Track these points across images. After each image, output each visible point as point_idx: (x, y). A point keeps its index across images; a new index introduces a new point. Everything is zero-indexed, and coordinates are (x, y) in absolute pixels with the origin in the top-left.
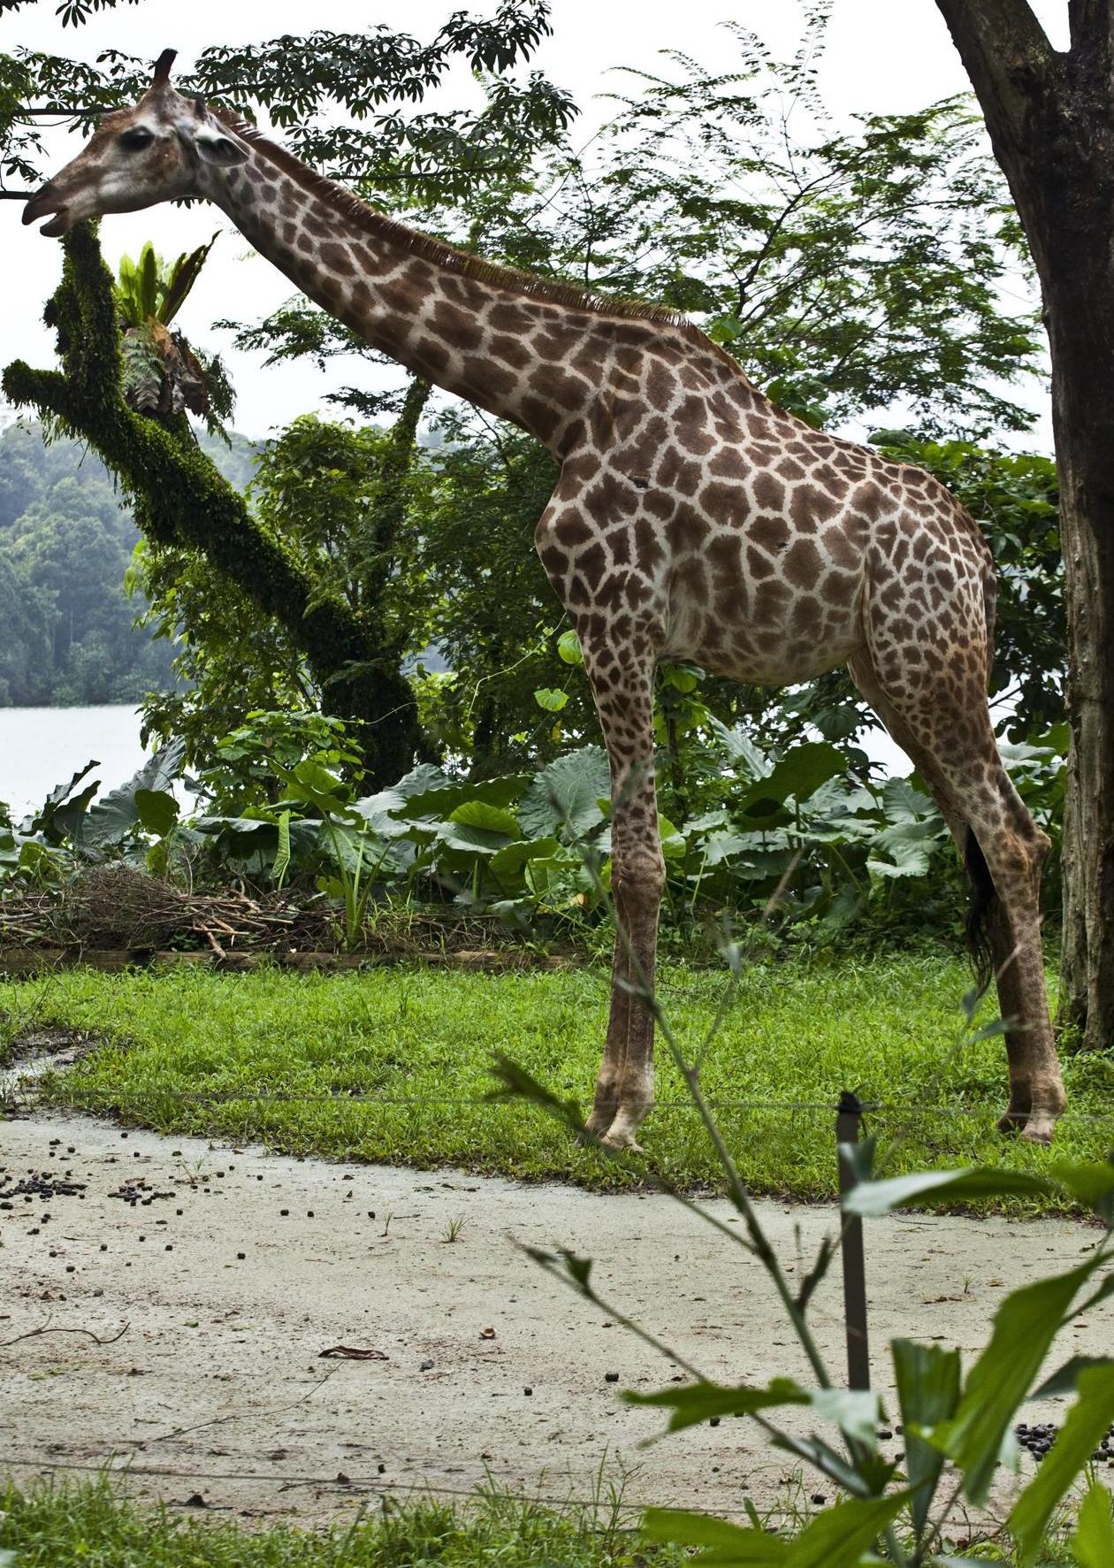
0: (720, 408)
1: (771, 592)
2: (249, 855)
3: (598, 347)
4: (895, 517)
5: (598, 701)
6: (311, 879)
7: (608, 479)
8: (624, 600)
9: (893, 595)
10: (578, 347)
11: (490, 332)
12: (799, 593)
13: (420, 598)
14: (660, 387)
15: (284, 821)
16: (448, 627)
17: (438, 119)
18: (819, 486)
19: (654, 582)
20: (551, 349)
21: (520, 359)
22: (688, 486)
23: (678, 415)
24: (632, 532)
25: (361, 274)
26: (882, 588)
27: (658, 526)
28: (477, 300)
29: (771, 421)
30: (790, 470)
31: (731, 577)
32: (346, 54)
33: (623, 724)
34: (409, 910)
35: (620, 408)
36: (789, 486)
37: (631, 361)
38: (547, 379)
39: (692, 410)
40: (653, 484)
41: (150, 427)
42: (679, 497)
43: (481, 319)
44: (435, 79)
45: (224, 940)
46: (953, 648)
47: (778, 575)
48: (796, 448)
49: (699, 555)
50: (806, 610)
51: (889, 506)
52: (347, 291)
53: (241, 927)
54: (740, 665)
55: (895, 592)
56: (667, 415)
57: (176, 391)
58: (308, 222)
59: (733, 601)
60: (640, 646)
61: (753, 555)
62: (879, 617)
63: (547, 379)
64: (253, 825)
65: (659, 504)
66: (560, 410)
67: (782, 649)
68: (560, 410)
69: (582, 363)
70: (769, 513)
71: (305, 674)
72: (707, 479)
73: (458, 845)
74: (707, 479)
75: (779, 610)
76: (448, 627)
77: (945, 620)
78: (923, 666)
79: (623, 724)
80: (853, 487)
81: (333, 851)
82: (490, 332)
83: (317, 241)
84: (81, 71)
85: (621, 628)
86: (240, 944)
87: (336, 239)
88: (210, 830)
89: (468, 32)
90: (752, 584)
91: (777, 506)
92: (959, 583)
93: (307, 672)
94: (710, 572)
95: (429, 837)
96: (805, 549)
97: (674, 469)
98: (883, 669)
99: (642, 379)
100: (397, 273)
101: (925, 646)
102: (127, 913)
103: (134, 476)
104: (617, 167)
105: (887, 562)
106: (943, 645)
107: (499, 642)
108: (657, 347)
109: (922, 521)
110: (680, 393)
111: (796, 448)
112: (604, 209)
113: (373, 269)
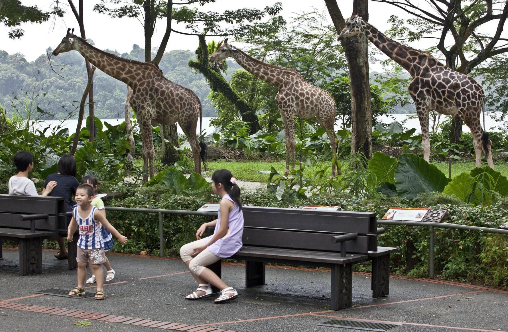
0: (300, 82)
1: (308, 106)
2: (232, 144)
3: (284, 75)
4: (323, 96)
5: (287, 121)
6: (242, 148)
7: (287, 92)
8: (290, 107)
9: (323, 107)
10: (281, 75)
11: (270, 73)
12: (311, 106)
13: (259, 101)
14: (293, 80)
15: (237, 139)
16: (264, 106)
17: (264, 23)
18: (314, 92)
19: (294, 105)
20: (278, 75)
21: (274, 76)
22: (297, 92)
23: (295, 83)
24: (290, 99)
25: (253, 67)
26: (322, 106)
27: (294, 97)
28: (268, 69)
29: (307, 84)
30: (310, 90)
31: (303, 105)
32: (249, 12)
33: (291, 123)
34: (258, 153)
35: (288, 82)
36: (310, 92)
37: (288, 76)
38: (278, 79)
39: (297, 82)
40: (293, 92)
41: (213, 71)
42: (296, 94)
43: (269, 72)
44: (263, 17)
45: (228, 158)
46: (330, 114)
47: (309, 104)
48: (310, 88)
49: (299, 101)
50: (312, 108)
51: (322, 95)
52: (251, 69)
53: (231, 155)
54: (303, 116)
55: (323, 107)
56: (294, 83)
57: (218, 65)
58: (246, 60)
59: (303, 107)
60: (293, 113)
61: (306, 101)
62: (321, 110)
63: (278, 79)
64: (233, 139)
65: (294, 95)
66: (280, 83)
67: (309, 113)
68: (280, 83)
69: (282, 77)
70: (308, 96)
71: (239, 114)
72: (299, 91)
73: (266, 143)
74: (299, 91)
75: (309, 109)
76: (264, 106)
77: (329, 110)
78: (326, 117)
79: (291, 123)
80: (318, 92)
81: (245, 144)
82: (270, 73)
83: (247, 63)
84: (204, 14)
85: (290, 111)
86: (231, 158)
87: (249, 62)
88: (225, 140)
89: (269, 9)
90: (305, 105)
91: (309, 95)
92: (331, 105)
93: (239, 114)
94: (300, 104)
95: (261, 141)
96: (312, 101)
97: (295, 90)
98: (321, 116)
99: (290, 79)
100: (257, 66)
101: (326, 114)
102: (213, 153)
103: (210, 80)
104: (293, 29)
105: (322, 102)
106: (329, 114)
107: (273, 109)
108: (292, 74)
109: (327, 97)
110: (295, 80)
111: (310, 88)
112: (291, 37)
113: (254, 66)
